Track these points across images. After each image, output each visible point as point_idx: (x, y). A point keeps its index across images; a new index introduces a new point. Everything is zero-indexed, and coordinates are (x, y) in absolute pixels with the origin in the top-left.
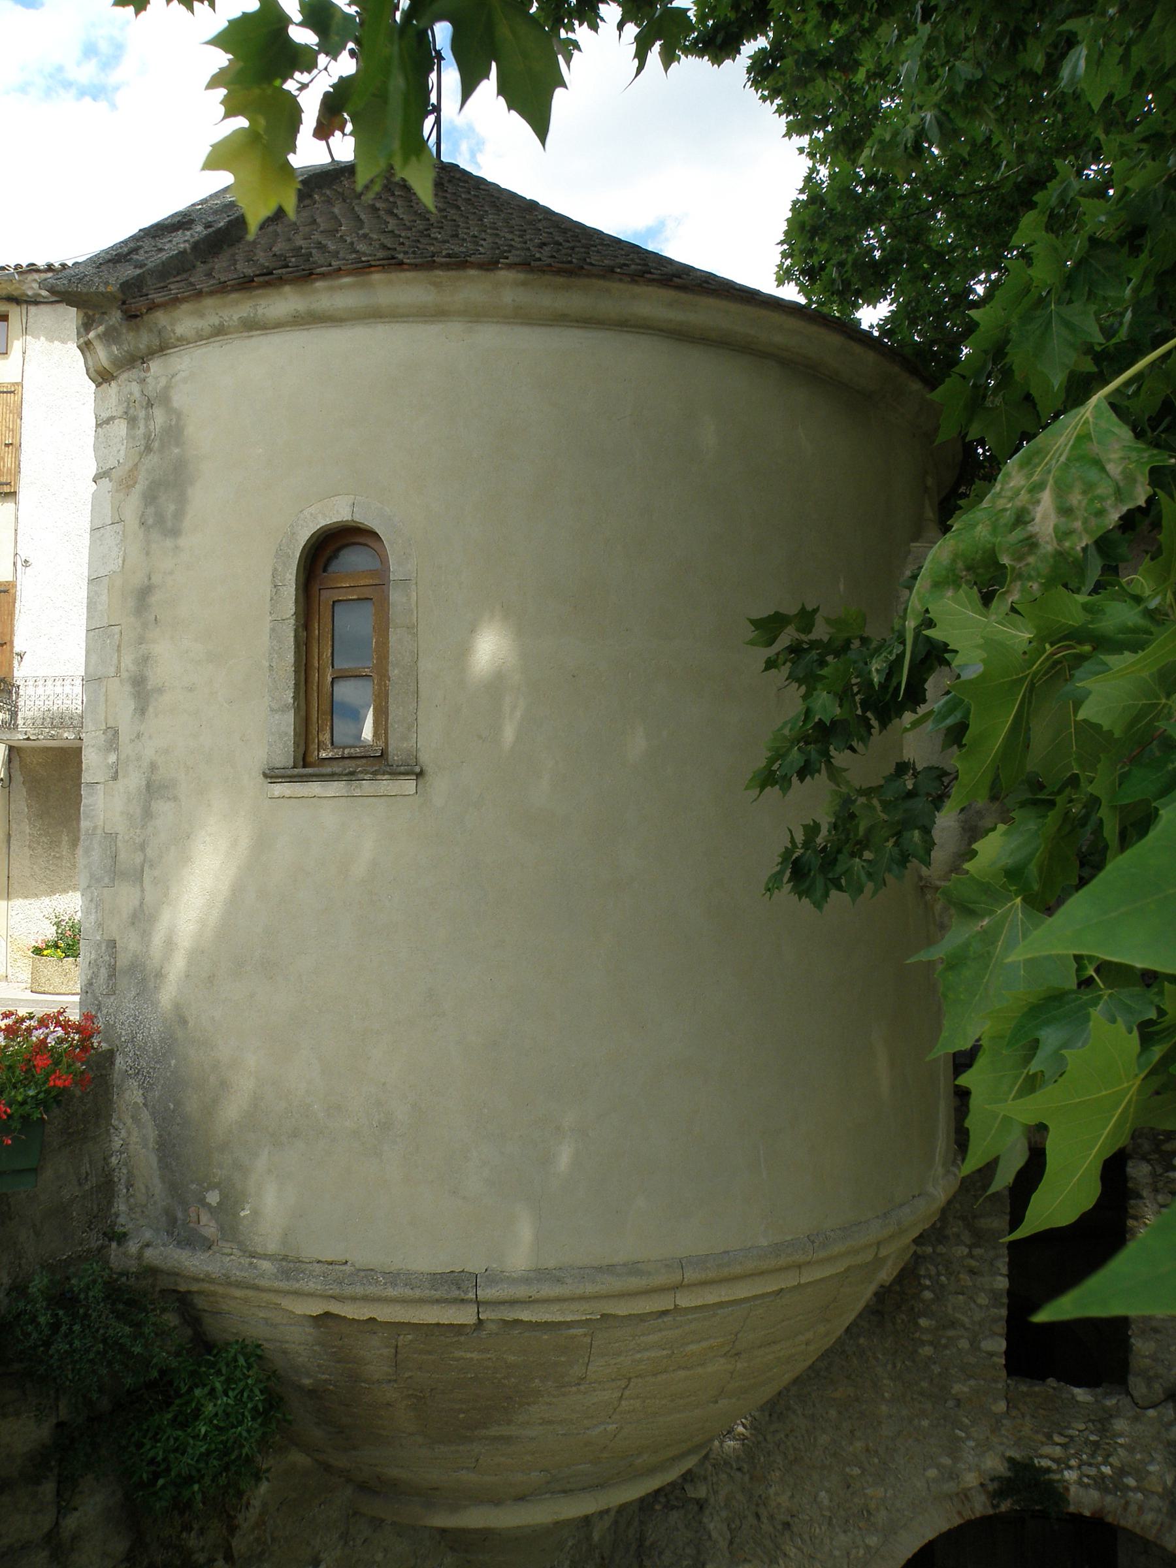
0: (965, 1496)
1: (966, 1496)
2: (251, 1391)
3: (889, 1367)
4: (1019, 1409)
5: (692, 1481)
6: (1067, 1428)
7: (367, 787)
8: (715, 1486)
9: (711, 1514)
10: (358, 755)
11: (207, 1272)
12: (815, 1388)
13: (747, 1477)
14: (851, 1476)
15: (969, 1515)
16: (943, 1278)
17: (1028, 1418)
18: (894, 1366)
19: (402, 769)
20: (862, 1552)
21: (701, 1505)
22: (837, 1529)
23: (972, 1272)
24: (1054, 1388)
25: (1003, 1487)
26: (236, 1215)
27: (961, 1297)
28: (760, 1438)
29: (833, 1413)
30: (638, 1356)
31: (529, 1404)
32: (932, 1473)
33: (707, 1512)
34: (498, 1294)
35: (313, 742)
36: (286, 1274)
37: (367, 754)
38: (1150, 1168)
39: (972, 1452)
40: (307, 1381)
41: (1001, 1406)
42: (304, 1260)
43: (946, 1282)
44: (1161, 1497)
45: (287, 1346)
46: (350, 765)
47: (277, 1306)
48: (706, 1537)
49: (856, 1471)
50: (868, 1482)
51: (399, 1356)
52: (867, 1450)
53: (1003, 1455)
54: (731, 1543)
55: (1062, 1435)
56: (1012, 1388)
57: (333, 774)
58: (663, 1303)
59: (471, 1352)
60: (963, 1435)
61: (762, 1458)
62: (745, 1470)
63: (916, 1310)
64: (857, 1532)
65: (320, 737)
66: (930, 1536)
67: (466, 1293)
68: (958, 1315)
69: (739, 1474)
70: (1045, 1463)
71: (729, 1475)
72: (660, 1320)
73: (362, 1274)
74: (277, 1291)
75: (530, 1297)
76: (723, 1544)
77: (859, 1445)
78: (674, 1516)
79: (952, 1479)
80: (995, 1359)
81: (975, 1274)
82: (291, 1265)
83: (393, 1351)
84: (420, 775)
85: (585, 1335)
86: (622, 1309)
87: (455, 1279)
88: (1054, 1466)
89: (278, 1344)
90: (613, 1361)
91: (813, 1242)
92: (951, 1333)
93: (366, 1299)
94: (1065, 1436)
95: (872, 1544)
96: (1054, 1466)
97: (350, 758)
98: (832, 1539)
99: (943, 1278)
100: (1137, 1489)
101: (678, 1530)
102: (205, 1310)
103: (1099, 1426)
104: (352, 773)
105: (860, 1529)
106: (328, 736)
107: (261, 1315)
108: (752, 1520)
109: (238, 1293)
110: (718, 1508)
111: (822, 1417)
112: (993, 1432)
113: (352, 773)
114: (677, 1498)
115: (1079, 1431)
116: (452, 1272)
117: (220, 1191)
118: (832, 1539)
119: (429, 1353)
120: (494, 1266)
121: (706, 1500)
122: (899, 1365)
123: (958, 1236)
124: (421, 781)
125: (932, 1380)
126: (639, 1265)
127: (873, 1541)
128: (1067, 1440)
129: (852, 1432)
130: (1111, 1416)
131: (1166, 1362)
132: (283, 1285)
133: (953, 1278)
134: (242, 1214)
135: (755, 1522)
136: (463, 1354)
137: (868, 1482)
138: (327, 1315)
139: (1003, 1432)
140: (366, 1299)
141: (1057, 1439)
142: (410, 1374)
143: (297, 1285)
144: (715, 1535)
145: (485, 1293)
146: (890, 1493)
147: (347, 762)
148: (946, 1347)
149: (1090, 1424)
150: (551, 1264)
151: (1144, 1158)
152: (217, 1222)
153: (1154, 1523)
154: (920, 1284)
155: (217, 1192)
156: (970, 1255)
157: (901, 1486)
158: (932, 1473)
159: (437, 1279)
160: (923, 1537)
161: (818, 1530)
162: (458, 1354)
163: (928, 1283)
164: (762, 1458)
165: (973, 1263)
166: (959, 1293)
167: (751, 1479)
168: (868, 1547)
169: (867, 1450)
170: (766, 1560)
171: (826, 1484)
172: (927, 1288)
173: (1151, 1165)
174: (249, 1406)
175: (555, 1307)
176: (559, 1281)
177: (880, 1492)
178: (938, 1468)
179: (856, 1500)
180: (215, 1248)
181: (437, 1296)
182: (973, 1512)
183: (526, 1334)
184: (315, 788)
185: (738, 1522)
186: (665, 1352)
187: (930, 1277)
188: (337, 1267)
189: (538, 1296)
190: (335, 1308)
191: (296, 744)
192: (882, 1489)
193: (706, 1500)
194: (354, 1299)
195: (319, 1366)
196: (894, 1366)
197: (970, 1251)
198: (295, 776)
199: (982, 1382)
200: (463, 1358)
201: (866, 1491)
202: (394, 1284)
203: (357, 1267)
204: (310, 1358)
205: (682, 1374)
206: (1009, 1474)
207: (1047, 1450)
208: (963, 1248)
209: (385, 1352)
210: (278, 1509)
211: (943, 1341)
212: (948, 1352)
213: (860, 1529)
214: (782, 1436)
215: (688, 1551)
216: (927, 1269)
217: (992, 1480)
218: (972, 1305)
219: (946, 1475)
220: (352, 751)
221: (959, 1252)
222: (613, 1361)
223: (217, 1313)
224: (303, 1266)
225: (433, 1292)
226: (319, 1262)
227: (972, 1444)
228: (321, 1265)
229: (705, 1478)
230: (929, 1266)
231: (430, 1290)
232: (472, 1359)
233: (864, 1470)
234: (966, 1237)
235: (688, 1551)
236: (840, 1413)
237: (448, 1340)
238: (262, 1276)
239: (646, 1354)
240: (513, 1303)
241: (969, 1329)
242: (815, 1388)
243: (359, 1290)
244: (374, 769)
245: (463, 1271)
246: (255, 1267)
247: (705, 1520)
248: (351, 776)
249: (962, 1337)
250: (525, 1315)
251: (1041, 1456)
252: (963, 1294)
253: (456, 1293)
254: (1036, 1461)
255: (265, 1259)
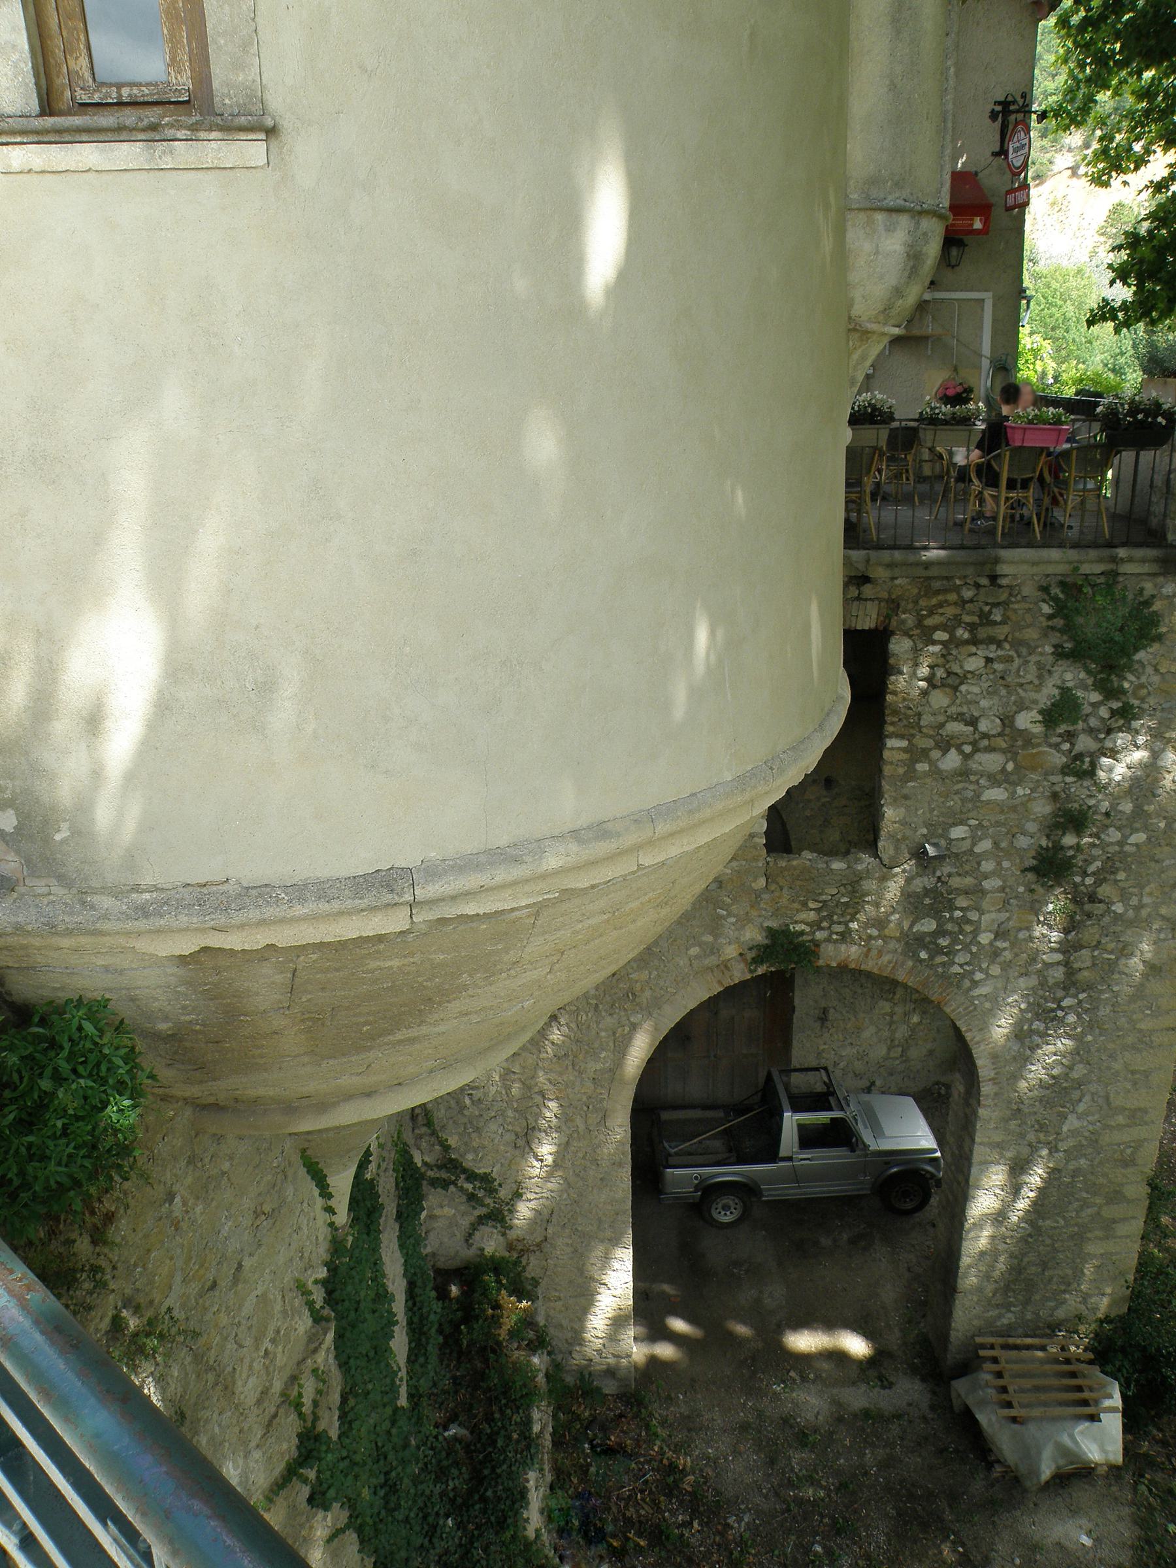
0: (725, 966)
1: (726, 967)
2: (110, 1061)
4: (777, 883)
6: (821, 894)
7: (182, 152)
10: (146, 99)
11: (18, 923)
15: (728, 982)
17: (785, 890)
19: (243, 120)
22: (604, 1014)
24: (810, 860)
25: (763, 953)
26: (47, 840)
31: (448, 1002)
32: (694, 951)
35: (59, 73)
37: (164, 98)
38: (912, 643)
39: (733, 928)
40: (163, 1026)
41: (762, 882)
44: (898, 940)
45: (138, 992)
46: (150, 115)
51: (296, 980)
53: (762, 926)
55: (816, 901)
56: (771, 864)
57: (120, 129)
59: (391, 960)
60: (725, 913)
64: (622, 1013)
65: (71, 63)
66: (692, 1005)
67: (400, 895)
70: (799, 927)
73: (254, 892)
74: (128, 934)
80: (757, 840)
83: (290, 975)
84: (271, 132)
86: (582, 881)
88: (808, 929)
89: (124, 992)
91: (772, 769)
93: (262, 923)
94: (820, 902)
96: (808, 929)
97: (134, 104)
98: (598, 1023)
100: (879, 937)
102: (8, 967)
103: (850, 888)
104: (153, 127)
105: (625, 1010)
106: (84, 62)
107: (100, 962)
109: (66, 942)
112: (752, 907)
113: (153, 127)
115: (832, 896)
117: (16, 810)
118: (598, 1023)
120: (433, 854)
124: (274, 143)
126: (604, 826)
128: (821, 905)
130: (861, 878)
131: (913, 825)
134: (58, 837)
138: (205, 949)
139: (762, 905)
141: (812, 905)
142: (309, 997)
147: (128, 111)
149: (842, 889)
150: (503, 841)
151: (907, 634)
152: (18, 852)
153: (890, 962)
155: (11, 812)
157: (665, 966)
158: (694, 951)
159: (361, 884)
160: (685, 1008)
161: (584, 1017)
162: (373, 964)
173: (913, 640)
174: (111, 1081)
176: (517, 860)
178: (700, 946)
180: (21, 889)
181: (363, 906)
184: (87, 154)
186: (605, 917)
188: (214, 888)
191: (37, 76)
198: (47, 132)
199: (744, 863)
202: (302, 900)
203: (245, 885)
204: (170, 1000)
206: (766, 942)
207: (803, 916)
213: (625, 1010)
217: (750, 949)
220: (135, 91)
223: (27, 968)
225: (357, 902)
227: (733, 920)
228: (190, 889)
231: (354, 899)
232: (391, 968)
238: (106, 917)
244: (193, 120)
245: (391, 868)
246: (92, 907)
248: (153, 133)
250: (470, 909)
251: (796, 922)
254: (791, 927)
255: (103, 893)
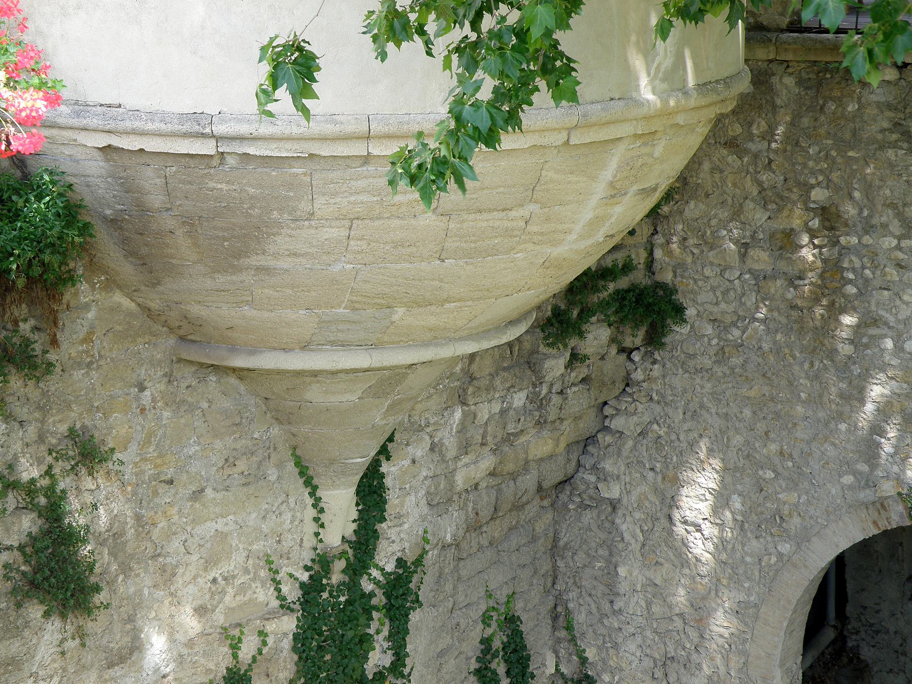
0: (881, 505)
1: (882, 505)
3: (806, 366)
5: (605, 480)
8: (628, 486)
9: (624, 515)
12: (730, 385)
13: (659, 478)
14: (764, 480)
15: (884, 525)
16: (867, 272)
18: (812, 364)
20: (774, 559)
21: (614, 505)
22: (749, 535)
23: (900, 266)
27: (886, 292)
28: (674, 437)
29: (747, 412)
30: (352, 199)
33: (620, 512)
34: (227, 130)
36: (78, 115)
40: (108, 212)
42: (90, 103)
43: (871, 276)
47: (75, 143)
48: (619, 539)
49: (770, 474)
50: (781, 487)
52: (781, 453)
54: (643, 545)
58: (358, 149)
61: (675, 458)
62: (658, 470)
63: (837, 305)
64: (769, 539)
66: (844, 545)
67: (204, 128)
68: (881, 313)
69: (651, 475)
71: (642, 474)
72: (365, 168)
73: (131, 113)
75: (251, 134)
76: (635, 546)
77: (773, 447)
78: (588, 517)
79: (869, 487)
81: (902, 267)
82: (82, 107)
85: (305, 174)
86: (325, 150)
87: (196, 116)
90: (333, 201)
92: (873, 331)
93: (134, 132)
95: (783, 551)
98: (743, 545)
99: (867, 272)
101: (591, 530)
108: (664, 522)
110: (630, 508)
111: (736, 416)
114: (591, 498)
116: (195, 113)
118: (743, 545)
119: (190, 183)
121: (619, 500)
122: (817, 364)
123: (885, 226)
125: (850, 383)
127: (785, 548)
129: (766, 433)
132: (75, 122)
133: (878, 272)
135: (667, 524)
136: (215, 185)
137: (781, 487)
140: (134, 132)
143: (85, 122)
144: (627, 537)
145: (220, 129)
146: (804, 498)
148: (867, 346)
154: (843, 278)
156: (898, 248)
157: (816, 492)
158: (848, 479)
159: (183, 117)
162: (211, 185)
163: (851, 276)
164: (675, 458)
165: (901, 255)
166: (885, 289)
167: (664, 479)
168: (780, 555)
169: (781, 453)
170: (677, 563)
171: (739, 487)
172: (850, 282)
175: (274, 145)
177: (793, 497)
178: (854, 476)
179: (768, 505)
182: (889, 523)
183: (259, 170)
185: (650, 525)
186: (375, 199)
187: (854, 270)
189: (255, 134)
190: (116, 142)
192: (796, 495)
193: (619, 500)
194: (127, 133)
195: (114, 196)
196: (812, 364)
197: (899, 243)
200: (215, 189)
201: (780, 496)
205: (396, 222)
208: (891, 239)
209: (157, 181)
210: (105, 334)
211: (865, 340)
212: (869, 351)
214: (696, 435)
215: (601, 552)
216: (851, 261)
218: (898, 302)
219: (863, 483)
221: (887, 243)
222: (333, 201)
224: (89, 108)
226: (101, 105)
229: (618, 477)
230: (854, 258)
232: (221, 189)
233: (777, 474)
234: (896, 227)
235: (601, 552)
236: (754, 413)
237: (202, 172)
239: (360, 198)
240: (241, 139)
241: (894, 327)
242: (730, 385)
243: (128, 124)
245: (203, 113)
247: (618, 521)
249: (885, 336)
252: (888, 290)
253: (196, 128)
